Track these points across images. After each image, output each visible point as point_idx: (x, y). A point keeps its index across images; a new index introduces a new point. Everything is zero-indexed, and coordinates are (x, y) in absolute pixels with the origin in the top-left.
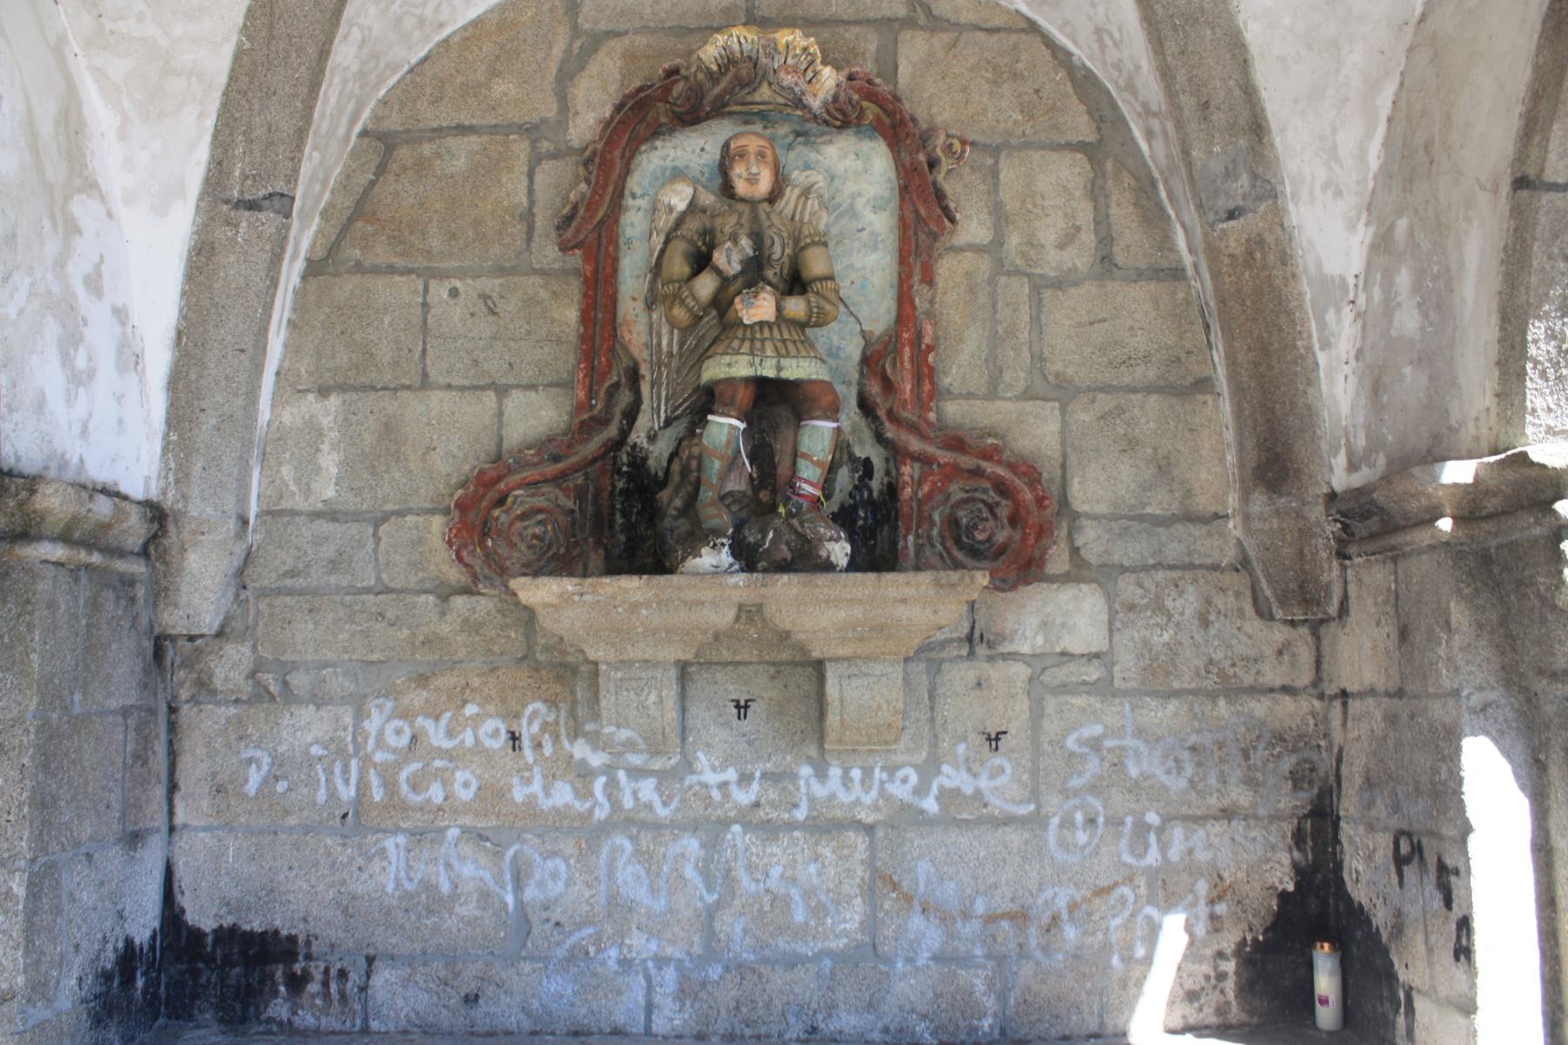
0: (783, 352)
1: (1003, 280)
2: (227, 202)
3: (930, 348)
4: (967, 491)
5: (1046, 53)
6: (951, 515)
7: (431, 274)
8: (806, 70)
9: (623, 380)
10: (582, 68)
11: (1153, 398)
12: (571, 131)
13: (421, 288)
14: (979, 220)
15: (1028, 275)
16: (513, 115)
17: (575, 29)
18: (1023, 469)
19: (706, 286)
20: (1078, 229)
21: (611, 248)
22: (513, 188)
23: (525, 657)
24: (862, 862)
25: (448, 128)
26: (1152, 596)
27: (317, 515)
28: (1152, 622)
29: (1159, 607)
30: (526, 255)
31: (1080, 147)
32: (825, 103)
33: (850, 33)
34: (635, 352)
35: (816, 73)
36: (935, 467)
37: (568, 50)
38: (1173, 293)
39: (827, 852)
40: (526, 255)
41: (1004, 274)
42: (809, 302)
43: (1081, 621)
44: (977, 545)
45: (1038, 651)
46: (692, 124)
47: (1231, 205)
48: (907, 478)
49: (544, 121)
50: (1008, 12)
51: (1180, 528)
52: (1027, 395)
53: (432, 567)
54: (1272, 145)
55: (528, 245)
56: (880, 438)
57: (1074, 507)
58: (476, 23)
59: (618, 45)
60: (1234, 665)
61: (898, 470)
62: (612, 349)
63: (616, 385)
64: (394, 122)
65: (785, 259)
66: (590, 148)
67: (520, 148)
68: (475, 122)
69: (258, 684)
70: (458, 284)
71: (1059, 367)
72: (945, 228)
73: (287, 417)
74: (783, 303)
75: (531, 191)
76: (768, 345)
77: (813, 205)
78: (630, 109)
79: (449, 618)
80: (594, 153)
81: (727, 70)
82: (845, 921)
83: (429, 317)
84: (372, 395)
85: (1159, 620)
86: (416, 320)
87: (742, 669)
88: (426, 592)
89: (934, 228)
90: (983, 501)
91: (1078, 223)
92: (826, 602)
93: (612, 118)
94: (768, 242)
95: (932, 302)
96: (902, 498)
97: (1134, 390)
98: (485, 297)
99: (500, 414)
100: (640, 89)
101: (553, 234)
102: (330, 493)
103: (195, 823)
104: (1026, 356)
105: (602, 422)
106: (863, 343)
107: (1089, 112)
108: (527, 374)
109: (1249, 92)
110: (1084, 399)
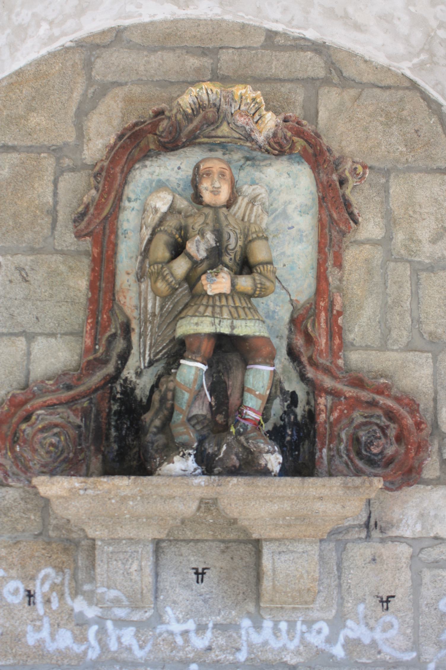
0: (236, 315)
1: (392, 265)
3: (340, 313)
5: (424, 104)
6: (354, 434)
8: (254, 114)
9: (119, 332)
10: (94, 108)
12: (86, 152)
17: (90, 79)
18: (406, 401)
21: (113, 237)
23: (40, 534)
32: (267, 138)
34: (128, 312)
36: (342, 399)
37: (85, 95)
41: (392, 261)
42: (254, 280)
44: (372, 457)
45: (417, 536)
46: (173, 150)
49: (66, 144)
52: (409, 348)
55: (53, 233)
56: (303, 377)
59: (120, 92)
62: (111, 309)
63: (114, 336)
65: (238, 249)
66: (99, 165)
68: (16, 143)
71: (432, 328)
72: (350, 227)
74: (236, 280)
75: (55, 194)
76: (225, 311)
77: (258, 210)
80: (102, 169)
81: (198, 113)
87: (200, 545)
92: (264, 498)
93: (115, 144)
94: (226, 236)
95: (341, 280)
98: (20, 269)
99: (29, 354)
100: (136, 124)
101: (71, 226)
104: (408, 319)
105: (103, 362)
106: (291, 308)
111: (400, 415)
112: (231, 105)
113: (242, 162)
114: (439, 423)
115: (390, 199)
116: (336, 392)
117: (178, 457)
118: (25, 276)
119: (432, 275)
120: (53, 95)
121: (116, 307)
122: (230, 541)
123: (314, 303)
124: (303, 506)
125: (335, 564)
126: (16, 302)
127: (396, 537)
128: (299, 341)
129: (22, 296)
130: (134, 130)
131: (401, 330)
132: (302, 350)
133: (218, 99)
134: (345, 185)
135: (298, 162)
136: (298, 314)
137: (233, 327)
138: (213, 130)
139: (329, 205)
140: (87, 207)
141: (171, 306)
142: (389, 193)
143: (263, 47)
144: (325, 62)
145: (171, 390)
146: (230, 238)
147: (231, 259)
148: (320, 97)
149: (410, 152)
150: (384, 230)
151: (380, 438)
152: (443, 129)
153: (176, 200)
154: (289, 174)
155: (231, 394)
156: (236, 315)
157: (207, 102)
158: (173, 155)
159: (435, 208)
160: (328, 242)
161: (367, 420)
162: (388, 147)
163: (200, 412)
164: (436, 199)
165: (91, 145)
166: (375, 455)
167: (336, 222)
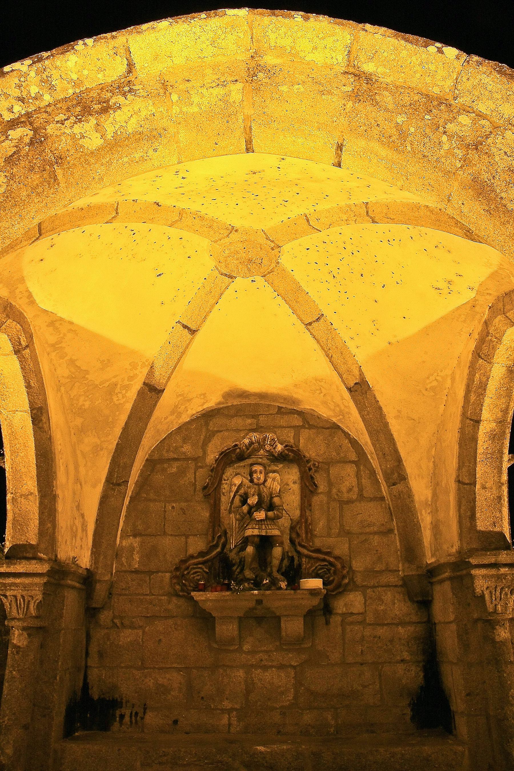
2: (112, 484)
5: (343, 435)
16: (189, 455)
19: (245, 508)
22: (190, 476)
24: (293, 678)
25: (171, 459)
27: (132, 572)
29: (380, 599)
35: (276, 446)
37: (206, 437)
39: (283, 675)
47: (393, 481)
49: (199, 457)
50: (331, 423)
52: (339, 535)
54: (403, 465)
60: (403, 616)
61: (301, 560)
62: (219, 526)
64: (156, 457)
65: (268, 501)
67: (192, 465)
69: (113, 622)
73: (124, 544)
75: (195, 478)
82: (288, 696)
97: (371, 534)
98: (182, 509)
99: (187, 543)
102: (137, 566)
103: (93, 665)
104: (338, 524)
105: (216, 546)
109: (396, 451)
128: (294, 536)
137: (266, 532)
143: (277, 413)
144: (302, 419)
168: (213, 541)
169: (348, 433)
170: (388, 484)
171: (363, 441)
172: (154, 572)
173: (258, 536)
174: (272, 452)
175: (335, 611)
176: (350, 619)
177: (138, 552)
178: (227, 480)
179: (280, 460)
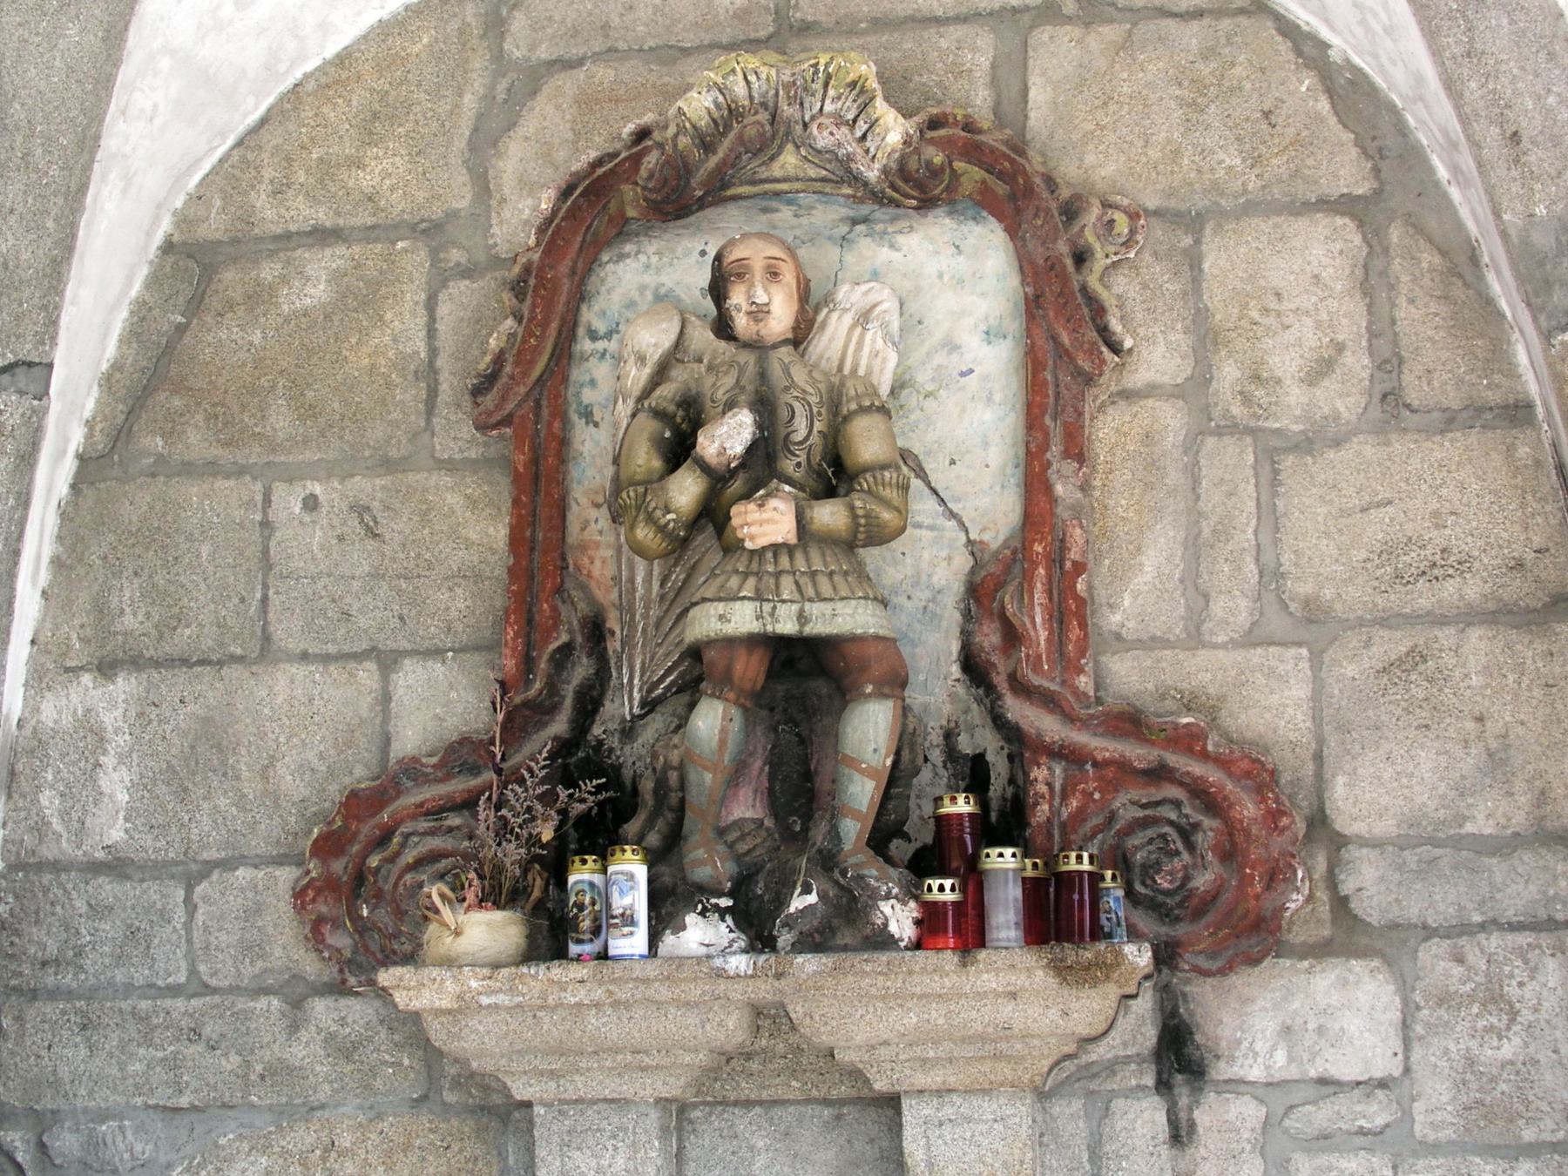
0: (810, 592)
1: (1211, 442)
3: (1079, 568)
4: (1144, 806)
5: (1284, 46)
6: (1117, 847)
7: (274, 473)
8: (855, 121)
9: (579, 639)
10: (511, 126)
11: (1475, 633)
12: (495, 230)
13: (259, 498)
14: (1168, 343)
15: (1252, 432)
16: (397, 205)
17: (499, 56)
18: (1245, 765)
20: (1340, 348)
21: (557, 425)
23: (424, 1098)
26: (1480, 979)
27: (95, 868)
28: (1481, 1023)
29: (1494, 997)
30: (426, 437)
31: (1344, 205)
32: (885, 171)
33: (947, 39)
34: (599, 594)
36: (1088, 767)
37: (488, 97)
38: (1511, 449)
40: (426, 437)
41: (1212, 433)
42: (852, 508)
43: (1353, 1024)
44: (1160, 898)
45: (1278, 1077)
46: (678, 217)
48: (1042, 788)
49: (453, 215)
51: (1527, 860)
52: (1252, 638)
53: (278, 952)
55: (428, 421)
56: (999, 722)
57: (1338, 827)
58: (343, 59)
59: (567, 84)
61: (1026, 774)
62: (559, 590)
63: (566, 650)
64: (214, 226)
65: (815, 439)
66: (522, 260)
67: (414, 260)
68: (341, 222)
70: (317, 489)
71: (1306, 588)
72: (1103, 362)
73: (49, 712)
74: (808, 513)
75: (431, 333)
76: (787, 583)
77: (874, 341)
78: (581, 195)
79: (304, 1035)
80: (527, 269)
81: (728, 127)
83: (273, 543)
84: (182, 675)
85: (1494, 1020)
86: (253, 551)
87: (777, 1112)
88: (266, 991)
89: (1085, 365)
90: (1171, 823)
91: (1340, 338)
92: (883, 998)
93: (555, 212)
94: (784, 414)
95: (1085, 488)
96: (1034, 821)
97: (1442, 621)
98: (360, 509)
99: (386, 698)
100: (599, 162)
101: (467, 401)
102: (116, 835)
104: (1251, 569)
105: (542, 710)
106: (971, 562)
107: (1358, 143)
108: (432, 630)
110: (1353, 640)
111: (1225, 798)
112: (802, 104)
113: (844, 229)
114: (1328, 812)
115: (1205, 285)
116: (1073, 752)
117: (693, 915)
118: (371, 524)
119: (1309, 460)
120: (419, 104)
121: (569, 585)
122: (842, 1102)
123: (1019, 546)
124: (974, 1014)
125: (1084, 1147)
126: (355, 583)
127: (1227, 1082)
128: (989, 637)
129: (367, 568)
130: (595, 176)
131: (1234, 597)
132: (994, 659)
133: (772, 92)
134: (1087, 264)
135: (974, 219)
136: (983, 573)
137: (802, 618)
138: (764, 163)
139: (1051, 314)
140: (499, 360)
141: (682, 577)
142: (1201, 270)
145: (675, 768)
146: (793, 417)
147: (799, 465)
148: (1031, 53)
149: (1252, 166)
150: (1191, 361)
151: (1177, 853)
152: (1333, 105)
153: (689, 330)
154: (957, 247)
155: (816, 769)
156: (810, 592)
157: (747, 103)
158: (684, 227)
159: (1314, 299)
160: (1051, 400)
161: (1148, 812)
162: (1197, 158)
163: (749, 815)
164: (1316, 277)
165: (506, 214)
166: (1167, 893)
167: (1067, 351)
168: (528, 683)
169: (1313, 38)
170: (1542, 318)
171: (1400, 76)
172: (210, 867)
173: (755, 641)
174: (850, 158)
175: (1221, 1071)
176: (1321, 1115)
177: (123, 759)
178: (609, 335)
179: (892, 201)
